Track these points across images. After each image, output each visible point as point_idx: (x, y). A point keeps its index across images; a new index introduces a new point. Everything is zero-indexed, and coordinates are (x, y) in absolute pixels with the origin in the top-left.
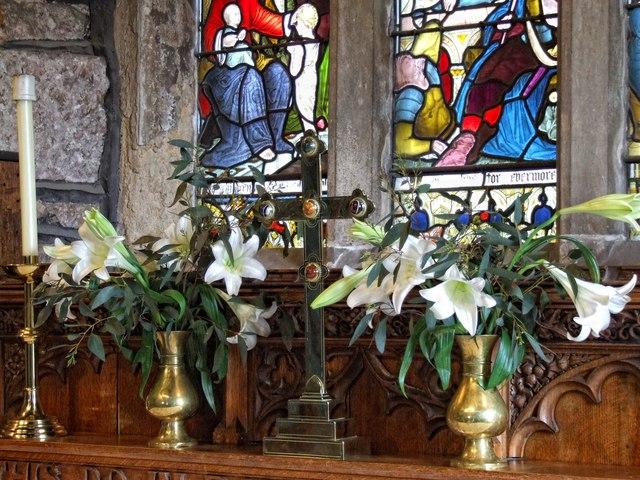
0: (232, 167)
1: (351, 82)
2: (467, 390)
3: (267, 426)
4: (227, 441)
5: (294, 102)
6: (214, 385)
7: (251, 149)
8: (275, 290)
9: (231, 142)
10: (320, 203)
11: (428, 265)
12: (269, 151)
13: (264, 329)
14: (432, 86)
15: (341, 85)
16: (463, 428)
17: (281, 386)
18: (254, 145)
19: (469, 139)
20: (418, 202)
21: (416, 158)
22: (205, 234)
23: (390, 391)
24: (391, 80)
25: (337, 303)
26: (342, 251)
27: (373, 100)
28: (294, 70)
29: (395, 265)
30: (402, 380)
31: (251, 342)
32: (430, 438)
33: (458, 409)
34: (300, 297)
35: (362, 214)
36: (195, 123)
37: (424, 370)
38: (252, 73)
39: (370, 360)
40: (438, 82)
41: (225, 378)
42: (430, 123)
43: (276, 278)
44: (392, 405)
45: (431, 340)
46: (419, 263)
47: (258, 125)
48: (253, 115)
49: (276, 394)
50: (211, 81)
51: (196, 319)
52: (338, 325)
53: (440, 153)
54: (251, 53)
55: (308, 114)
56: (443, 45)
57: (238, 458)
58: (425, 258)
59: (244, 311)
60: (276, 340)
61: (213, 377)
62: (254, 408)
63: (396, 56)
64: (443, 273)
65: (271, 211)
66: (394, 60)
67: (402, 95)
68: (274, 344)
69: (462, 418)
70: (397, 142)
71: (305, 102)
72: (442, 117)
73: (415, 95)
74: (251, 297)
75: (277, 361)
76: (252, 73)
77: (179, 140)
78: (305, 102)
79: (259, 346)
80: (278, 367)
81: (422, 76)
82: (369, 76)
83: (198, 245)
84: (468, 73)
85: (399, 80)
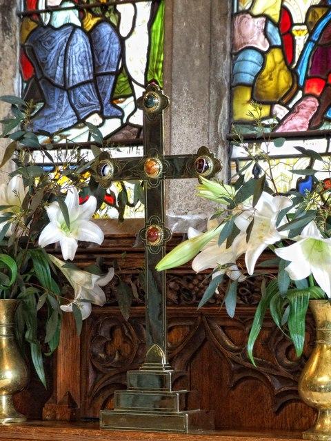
0: (57, 133)
1: (187, 41)
2: (321, 358)
3: (100, 401)
4: (58, 417)
5: (124, 65)
6: (44, 357)
7: (77, 114)
8: (111, 256)
9: (56, 107)
10: (162, 161)
11: (283, 223)
12: (96, 116)
13: (99, 298)
14: (272, 47)
15: (177, 45)
16: (317, 398)
17: (116, 358)
18: (80, 110)
19: (312, 103)
20: (257, 170)
21: (253, 124)
22: (40, 194)
23: (234, 362)
24: (228, 41)
25: (183, 265)
26: (176, 220)
27: (210, 62)
28: (124, 31)
29: (246, 224)
30: (250, 348)
31: (86, 310)
32: (277, 413)
33: (312, 377)
34: (139, 263)
35: (208, 173)
36: (16, 87)
37: (275, 337)
38: (79, 33)
39: (213, 330)
40: (279, 43)
41: (56, 350)
42: (270, 86)
43: (112, 243)
44: (237, 377)
45: (284, 303)
46: (274, 220)
47: (84, 89)
48: (79, 78)
49: (111, 367)
50: (35, 43)
51: (27, 286)
52: (179, 293)
53: (281, 118)
54: (77, 12)
55: (139, 77)
56: (285, 4)
57: (73, 432)
58: (280, 216)
59: (78, 278)
60: (111, 310)
61: (44, 348)
62: (87, 383)
63: (233, 16)
64: (298, 232)
65: (111, 171)
66: (232, 18)
67: (240, 57)
68: (109, 314)
69: (315, 388)
70: (232, 105)
71: (136, 65)
72: (284, 80)
73: (253, 57)
74: (86, 264)
75: (112, 331)
76: (79, 33)
77: (9, 97)
78: (136, 65)
79: (93, 316)
80: (113, 339)
81: (262, 36)
82: (206, 35)
83: (33, 207)
84: (311, 33)
85: (238, 41)
